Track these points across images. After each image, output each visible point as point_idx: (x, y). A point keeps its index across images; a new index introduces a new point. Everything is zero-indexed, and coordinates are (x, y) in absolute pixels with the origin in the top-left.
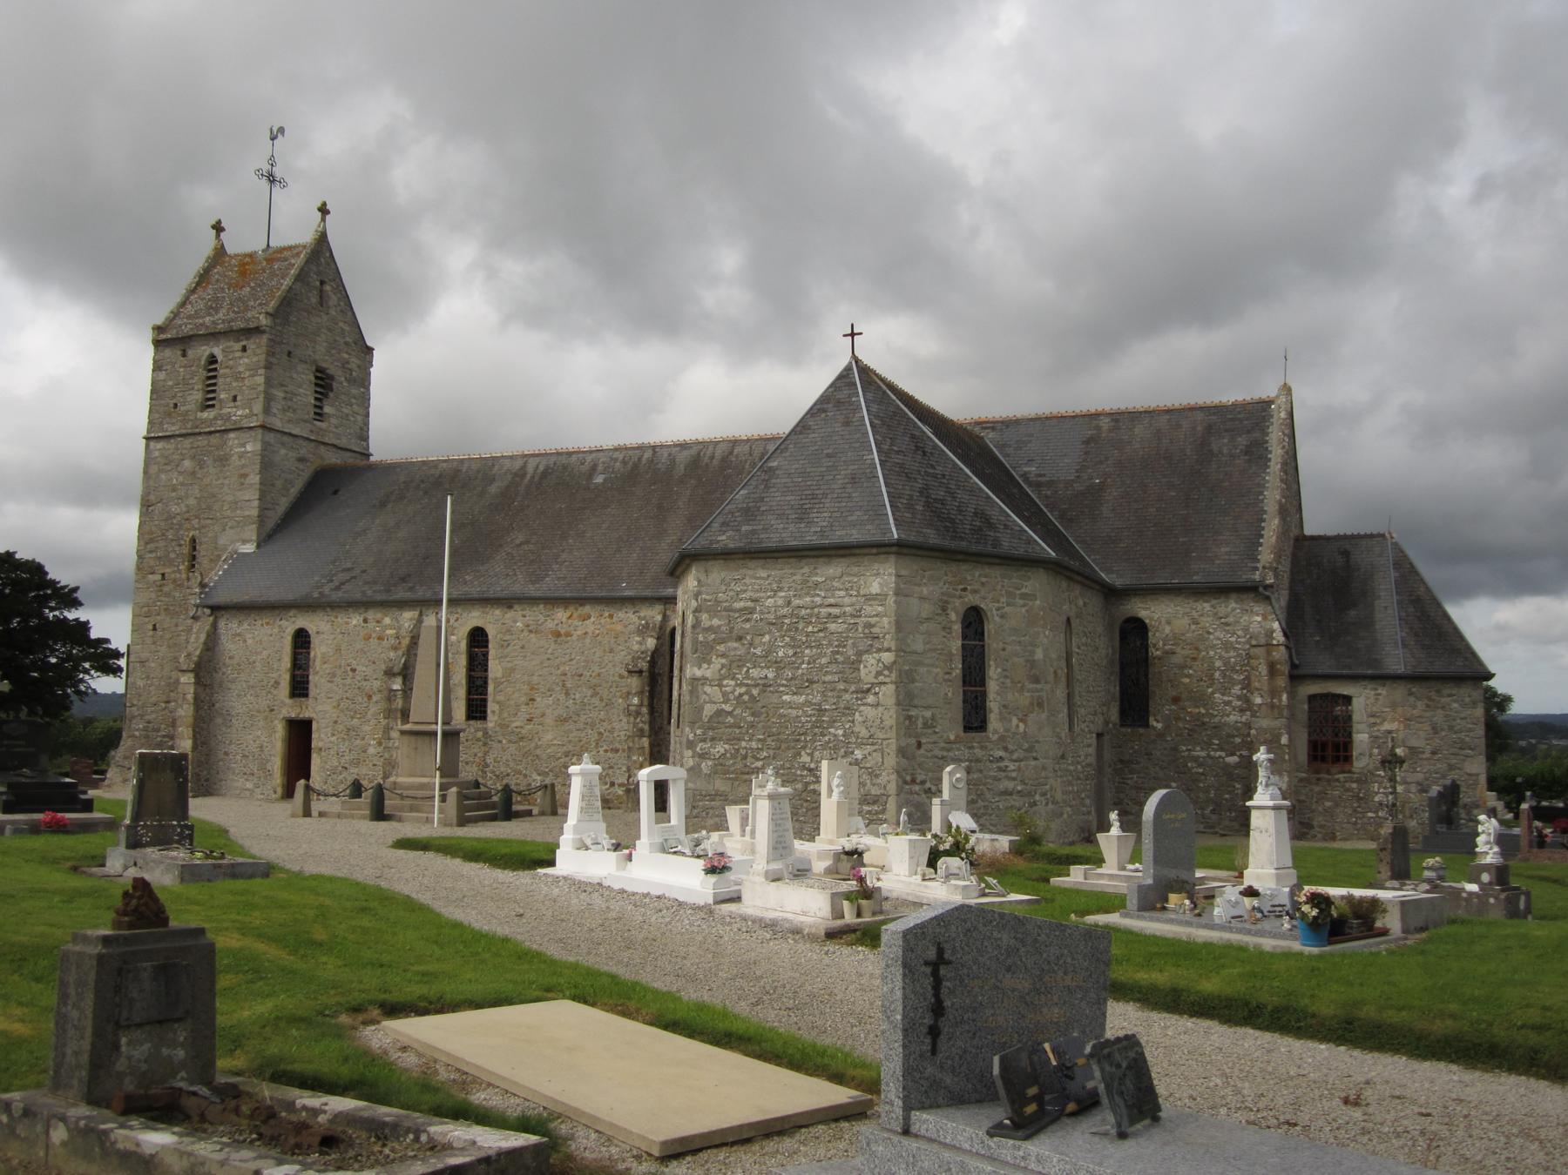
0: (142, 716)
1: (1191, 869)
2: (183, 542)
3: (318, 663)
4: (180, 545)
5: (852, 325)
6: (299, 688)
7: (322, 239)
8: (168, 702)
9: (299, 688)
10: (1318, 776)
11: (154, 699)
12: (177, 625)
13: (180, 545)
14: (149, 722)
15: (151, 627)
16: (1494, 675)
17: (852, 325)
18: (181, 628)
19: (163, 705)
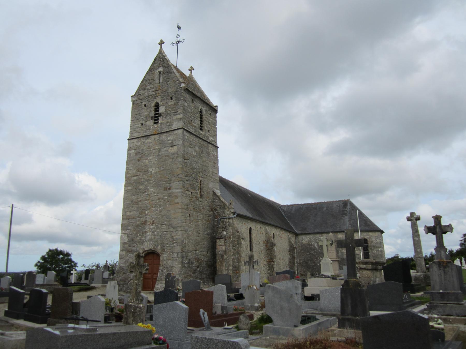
0: (187, 257)
1: (254, 304)
2: (198, 181)
3: (254, 240)
4: (197, 182)
5: (178, 24)
6: (251, 250)
7: (161, 52)
8: (196, 251)
9: (251, 250)
10: (426, 274)
11: (191, 249)
12: (198, 217)
13: (197, 182)
14: (190, 260)
15: (188, 215)
16: (433, 217)
17: (178, 24)
18: (199, 218)
19: (194, 252)
